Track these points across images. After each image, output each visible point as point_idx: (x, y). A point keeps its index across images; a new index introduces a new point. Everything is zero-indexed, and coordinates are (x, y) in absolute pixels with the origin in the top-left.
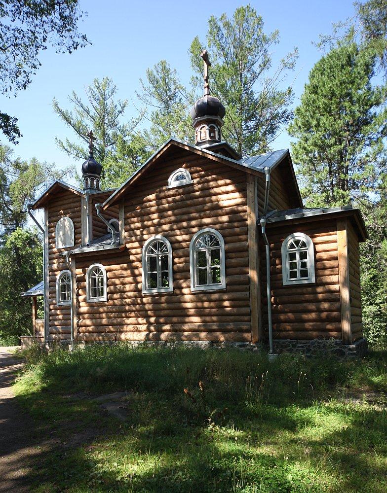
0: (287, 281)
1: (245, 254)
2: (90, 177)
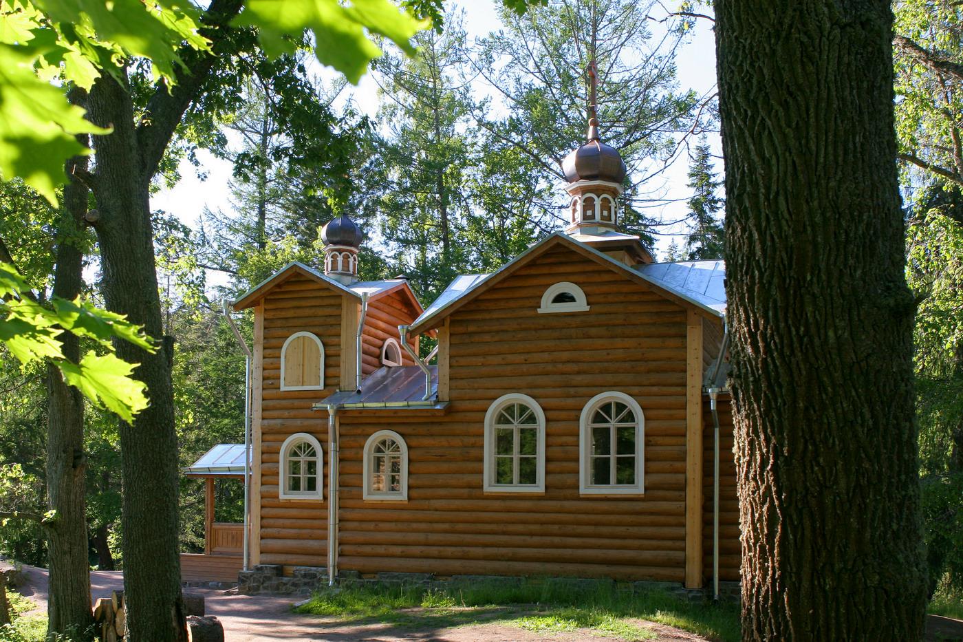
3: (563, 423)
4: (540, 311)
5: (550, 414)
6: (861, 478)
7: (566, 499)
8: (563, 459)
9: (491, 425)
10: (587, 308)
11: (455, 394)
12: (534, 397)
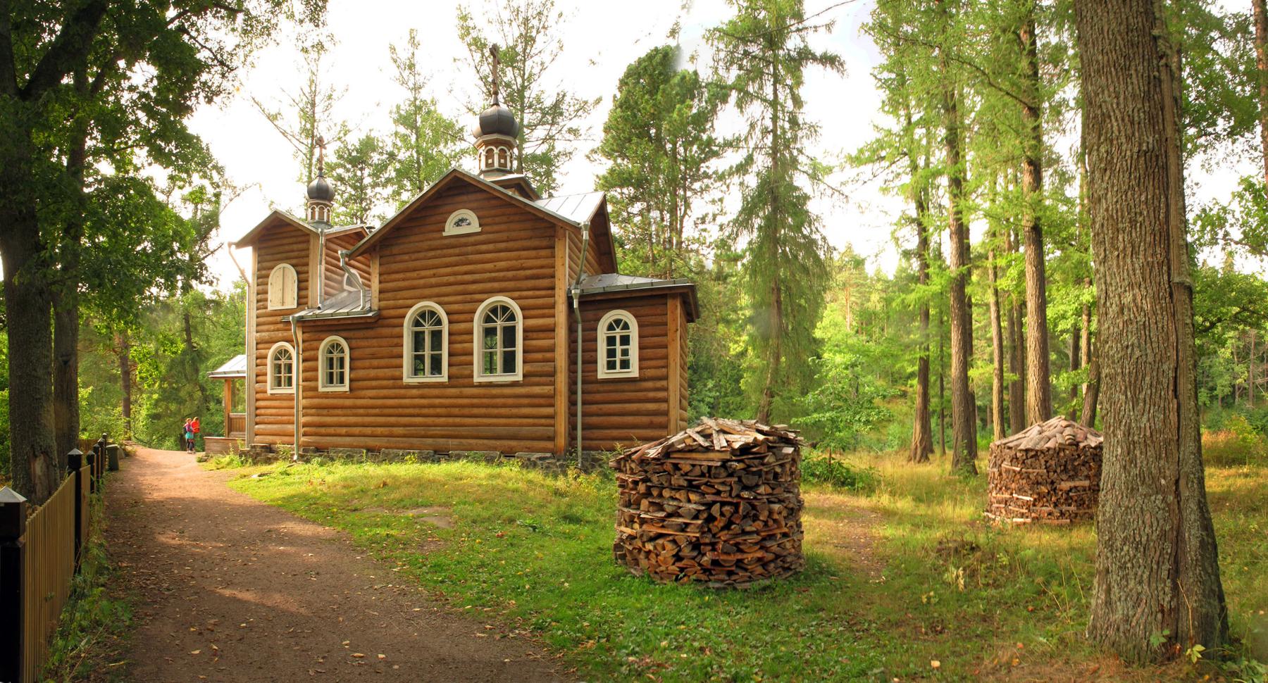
0: (602, 373)
1: (550, 334)
2: (317, 204)
3: (286, 295)
4: (444, 234)
5: (452, 317)
6: (1156, 148)
7: (465, 386)
8: (461, 357)
9: (408, 328)
10: (479, 230)
11: (383, 303)
12: (440, 304)
